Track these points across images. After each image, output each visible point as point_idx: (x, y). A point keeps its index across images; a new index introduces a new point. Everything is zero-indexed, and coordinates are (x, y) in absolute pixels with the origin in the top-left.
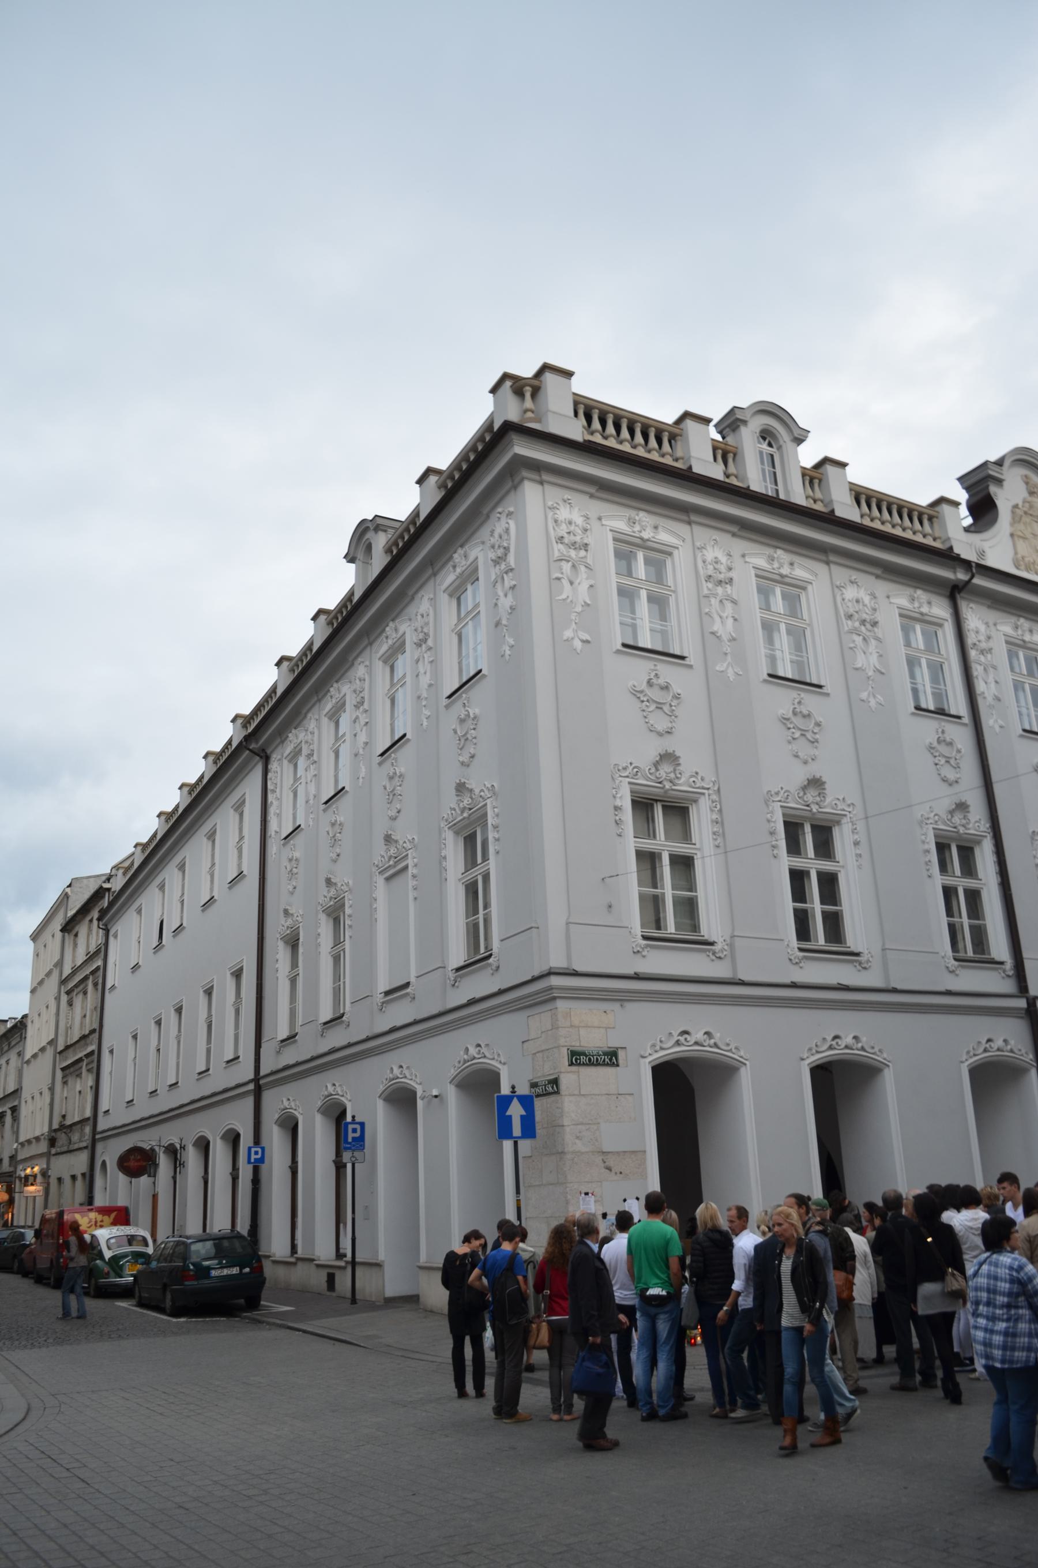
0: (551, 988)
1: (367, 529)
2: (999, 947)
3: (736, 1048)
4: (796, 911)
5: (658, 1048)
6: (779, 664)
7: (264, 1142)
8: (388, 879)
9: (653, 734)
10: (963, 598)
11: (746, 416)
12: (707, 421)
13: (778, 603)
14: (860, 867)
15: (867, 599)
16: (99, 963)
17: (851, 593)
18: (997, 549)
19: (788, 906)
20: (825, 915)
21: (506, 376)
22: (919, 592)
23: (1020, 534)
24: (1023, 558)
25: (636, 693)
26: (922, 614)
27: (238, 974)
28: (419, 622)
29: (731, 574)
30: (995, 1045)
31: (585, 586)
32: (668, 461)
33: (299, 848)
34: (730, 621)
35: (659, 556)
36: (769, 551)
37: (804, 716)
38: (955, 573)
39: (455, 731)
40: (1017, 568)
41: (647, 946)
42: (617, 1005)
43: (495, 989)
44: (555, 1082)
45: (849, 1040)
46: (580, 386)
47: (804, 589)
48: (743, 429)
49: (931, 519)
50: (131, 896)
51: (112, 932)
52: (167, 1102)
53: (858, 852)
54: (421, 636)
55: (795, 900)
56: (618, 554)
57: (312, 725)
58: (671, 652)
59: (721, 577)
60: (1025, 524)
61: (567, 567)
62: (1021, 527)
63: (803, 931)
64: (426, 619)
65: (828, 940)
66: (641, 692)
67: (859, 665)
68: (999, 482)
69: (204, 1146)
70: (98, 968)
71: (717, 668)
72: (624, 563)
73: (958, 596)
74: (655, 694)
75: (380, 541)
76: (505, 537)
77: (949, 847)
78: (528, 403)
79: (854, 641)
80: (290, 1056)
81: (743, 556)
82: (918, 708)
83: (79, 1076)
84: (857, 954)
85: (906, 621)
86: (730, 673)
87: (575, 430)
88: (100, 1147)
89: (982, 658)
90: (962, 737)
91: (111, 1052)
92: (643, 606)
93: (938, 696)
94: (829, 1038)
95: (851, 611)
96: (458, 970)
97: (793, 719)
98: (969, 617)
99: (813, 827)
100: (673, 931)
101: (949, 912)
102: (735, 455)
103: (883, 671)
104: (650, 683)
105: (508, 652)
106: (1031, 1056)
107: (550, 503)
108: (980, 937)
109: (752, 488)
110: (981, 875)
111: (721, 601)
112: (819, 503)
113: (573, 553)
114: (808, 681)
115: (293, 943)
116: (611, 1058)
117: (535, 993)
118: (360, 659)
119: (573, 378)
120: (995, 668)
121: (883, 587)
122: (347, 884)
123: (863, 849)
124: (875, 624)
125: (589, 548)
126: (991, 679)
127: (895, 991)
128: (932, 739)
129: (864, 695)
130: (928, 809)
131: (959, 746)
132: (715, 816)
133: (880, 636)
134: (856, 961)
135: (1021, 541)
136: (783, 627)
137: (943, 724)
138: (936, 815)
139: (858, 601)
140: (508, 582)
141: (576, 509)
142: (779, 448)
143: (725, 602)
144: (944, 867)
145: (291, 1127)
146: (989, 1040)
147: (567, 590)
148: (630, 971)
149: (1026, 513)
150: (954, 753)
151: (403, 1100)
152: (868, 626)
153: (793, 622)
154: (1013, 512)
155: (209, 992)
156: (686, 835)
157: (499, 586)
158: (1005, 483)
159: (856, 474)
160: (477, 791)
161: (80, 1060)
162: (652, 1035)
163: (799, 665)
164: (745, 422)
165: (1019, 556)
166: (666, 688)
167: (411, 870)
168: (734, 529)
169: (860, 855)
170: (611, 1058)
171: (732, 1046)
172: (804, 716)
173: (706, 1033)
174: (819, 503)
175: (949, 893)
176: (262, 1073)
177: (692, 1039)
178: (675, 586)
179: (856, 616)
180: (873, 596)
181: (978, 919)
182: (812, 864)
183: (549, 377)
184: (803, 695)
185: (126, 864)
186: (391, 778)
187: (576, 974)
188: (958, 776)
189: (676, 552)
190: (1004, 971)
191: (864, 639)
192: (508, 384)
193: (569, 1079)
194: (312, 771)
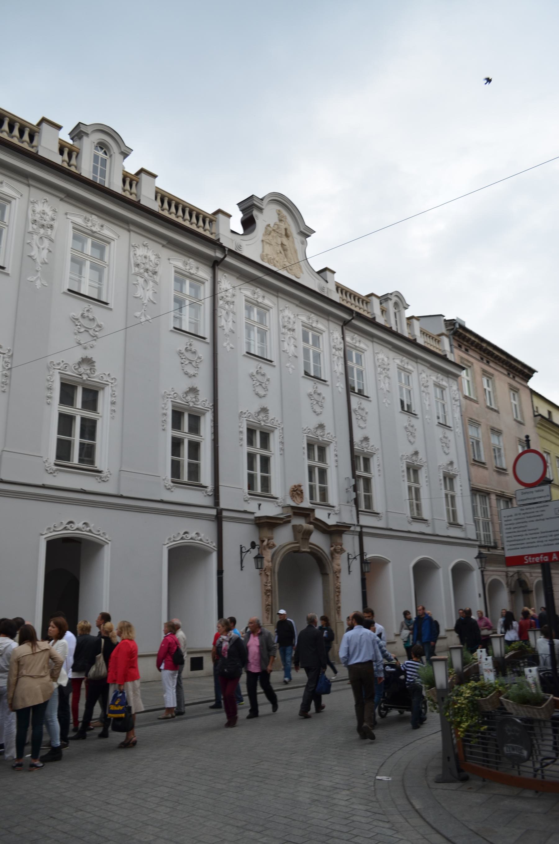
2: (206, 477)
3: (104, 533)
4: (173, 461)
5: (52, 530)
6: (183, 323)
9: (186, 376)
10: (219, 269)
11: (89, 131)
12: (59, 127)
13: (255, 316)
14: (113, 418)
15: (153, 258)
17: (141, 251)
18: (252, 248)
20: (190, 465)
22: (258, 290)
23: (268, 241)
24: (267, 255)
25: (180, 353)
26: (356, 346)
32: (207, 234)
34: (45, 252)
36: (186, 259)
37: (90, 320)
38: (215, 252)
40: (262, 260)
41: (57, 470)
46: (160, 183)
47: (268, 310)
48: (85, 138)
49: (367, 303)
53: (113, 408)
55: (173, 455)
56: (176, 280)
58: (199, 335)
60: (273, 237)
61: (36, 237)
62: (270, 237)
63: (251, 486)
65: (190, 478)
66: (77, 319)
67: (138, 296)
68: (260, 210)
71: (28, 279)
72: (179, 284)
73: (217, 268)
77: (255, 431)
79: (138, 281)
81: (66, 214)
82: (307, 373)
85: (179, 276)
86: (38, 284)
89: (227, 306)
90: (203, 351)
92: (87, 270)
93: (317, 369)
94: (182, 533)
95: (139, 262)
98: (223, 281)
99: (190, 415)
100: (186, 480)
101: (311, 479)
102: (78, 154)
103: (155, 302)
106: (214, 544)
107: (32, 199)
108: (194, 471)
109: (82, 175)
110: (202, 434)
111: (41, 238)
112: (134, 195)
114: (265, 357)
119: (157, 179)
121: (166, 253)
123: (381, 468)
124: (155, 273)
125: (235, 303)
127: (121, 497)
128: (254, 371)
129: (138, 314)
130: (170, 389)
131: (200, 355)
133: (158, 281)
134: (98, 476)
135: (268, 245)
136: (256, 328)
137: (192, 340)
138: (175, 393)
139: (145, 257)
141: (151, 251)
142: (111, 156)
143: (44, 238)
146: (186, 533)
147: (382, 385)
149: (274, 230)
150: (321, 399)
152: (150, 273)
154: (266, 228)
158: (264, 211)
159: (339, 278)
163: (262, 349)
164: (87, 134)
165: (264, 253)
169: (114, 411)
171: (101, 532)
172: (90, 320)
173: (84, 523)
174: (134, 195)
175: (251, 457)
177: (189, 536)
178: (109, 263)
179: (143, 266)
180: (158, 257)
181: (267, 473)
182: (316, 463)
183: (221, 216)
184: (92, 306)
188: (321, 410)
190: (206, 492)
191: (145, 280)
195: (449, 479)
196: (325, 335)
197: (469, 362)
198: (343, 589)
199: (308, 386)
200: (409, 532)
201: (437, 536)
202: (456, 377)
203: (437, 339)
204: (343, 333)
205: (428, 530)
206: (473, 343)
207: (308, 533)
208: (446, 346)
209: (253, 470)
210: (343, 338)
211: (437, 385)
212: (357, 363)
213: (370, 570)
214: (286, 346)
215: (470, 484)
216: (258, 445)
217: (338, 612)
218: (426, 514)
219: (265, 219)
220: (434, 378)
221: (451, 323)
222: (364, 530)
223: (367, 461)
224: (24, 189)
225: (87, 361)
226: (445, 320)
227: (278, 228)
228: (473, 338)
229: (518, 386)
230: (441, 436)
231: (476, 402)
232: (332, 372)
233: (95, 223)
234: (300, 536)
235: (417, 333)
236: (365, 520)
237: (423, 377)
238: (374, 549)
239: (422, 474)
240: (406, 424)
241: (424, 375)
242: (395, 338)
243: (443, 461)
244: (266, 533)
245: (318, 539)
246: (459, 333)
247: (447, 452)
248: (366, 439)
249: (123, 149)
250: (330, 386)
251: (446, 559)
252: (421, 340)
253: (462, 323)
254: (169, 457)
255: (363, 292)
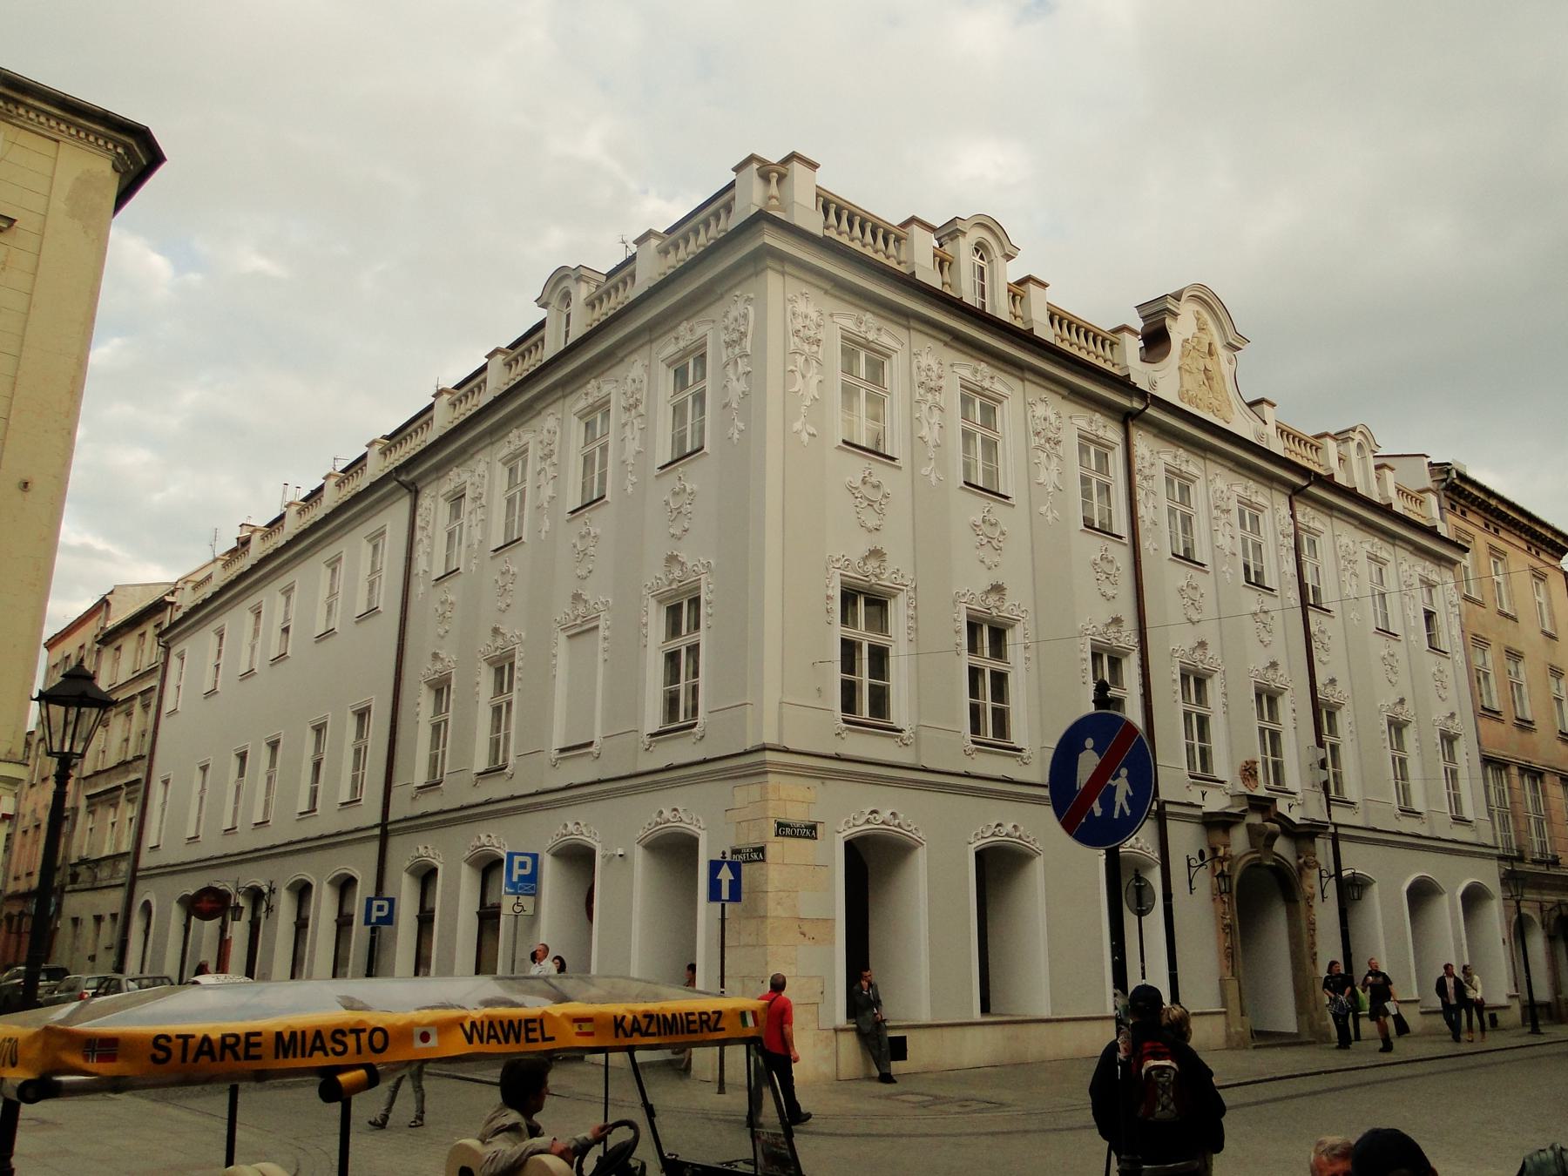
0: (764, 763)
1: (567, 276)
7: (388, 892)
8: (569, 637)
15: (1053, 418)
16: (154, 682)
17: (1040, 410)
19: (836, 675)
21: (752, 158)
22: (1098, 415)
25: (851, 489)
27: (362, 715)
28: (629, 387)
29: (942, 383)
30: (1004, 831)
31: (814, 381)
32: (892, 263)
33: (453, 591)
35: (878, 361)
39: (667, 503)
42: (818, 782)
43: (700, 757)
44: (761, 850)
45: (1009, 828)
49: (898, 240)
50: (206, 616)
51: (174, 651)
52: (247, 841)
54: (631, 401)
57: (481, 468)
59: (932, 384)
61: (800, 360)
62: (1188, 361)
63: (849, 704)
64: (637, 385)
69: (302, 891)
70: (152, 689)
74: (867, 491)
75: (582, 292)
76: (741, 321)
78: (774, 190)
80: (431, 803)
83: (115, 805)
84: (1020, 750)
85: (850, 346)
87: (813, 222)
88: (140, 886)
90: (1122, 555)
91: (166, 782)
96: (652, 735)
97: (862, 488)
99: (990, 629)
104: (864, 482)
105: (736, 436)
113: (806, 347)
115: (440, 688)
116: (810, 831)
117: (746, 764)
118: (550, 410)
120: (1154, 493)
122: (519, 637)
126: (1150, 505)
129: (1043, 509)
132: (911, 612)
140: (742, 366)
144: (973, 648)
145: (426, 877)
146: (873, 812)
147: (799, 385)
148: (832, 752)
151: (579, 858)
153: (989, 433)
155: (319, 729)
156: (883, 629)
157: (730, 369)
160: (689, 565)
161: (119, 788)
162: (848, 812)
164: (964, 233)
166: (877, 487)
167: (602, 633)
168: (947, 339)
170: (810, 831)
175: (975, 673)
176: (391, 818)
177: (880, 818)
182: (988, 664)
185: (199, 577)
186: (583, 537)
187: (787, 751)
189: (894, 356)
192: (755, 166)
193: (778, 848)
194: (480, 514)
195: (1449, 739)
196: (1200, 484)
197: (1466, 533)
198: (1318, 925)
199: (976, 507)
200: (968, 775)
201: (1374, 830)
202: (1452, 563)
203: (1417, 497)
204: (1292, 508)
205: (905, 757)
206: (1474, 500)
207: (1272, 837)
208: (1431, 510)
209: (852, 672)
210: (1293, 516)
211: (1373, 558)
212: (1099, 470)
213: (1351, 890)
214: (1221, 540)
215: (1480, 751)
216: (987, 653)
217: (1314, 962)
218: (1418, 804)
219: (1180, 331)
220: (1367, 546)
221: (1440, 469)
222: (1341, 831)
223: (1331, 715)
224: (1016, 384)
225: (876, 553)
226: (1430, 464)
227: (1199, 342)
228: (1476, 493)
229: (1547, 570)
230: (1434, 669)
231: (1481, 605)
232: (1281, 574)
233: (873, 328)
234: (1262, 841)
235: (1392, 493)
236: (1340, 815)
237: (1405, 567)
238: (1356, 859)
239: (1214, 688)
240: (1384, 652)
241: (1405, 566)
242: (1039, 355)
243: (1439, 713)
244: (1218, 836)
245: (1282, 847)
246: (1459, 490)
247: (1110, 593)
248: (1333, 681)
249: (1008, 249)
250: (1403, 643)
251: (1456, 876)
252: (1398, 507)
253: (1462, 470)
254: (1183, 741)
255: (893, 216)
